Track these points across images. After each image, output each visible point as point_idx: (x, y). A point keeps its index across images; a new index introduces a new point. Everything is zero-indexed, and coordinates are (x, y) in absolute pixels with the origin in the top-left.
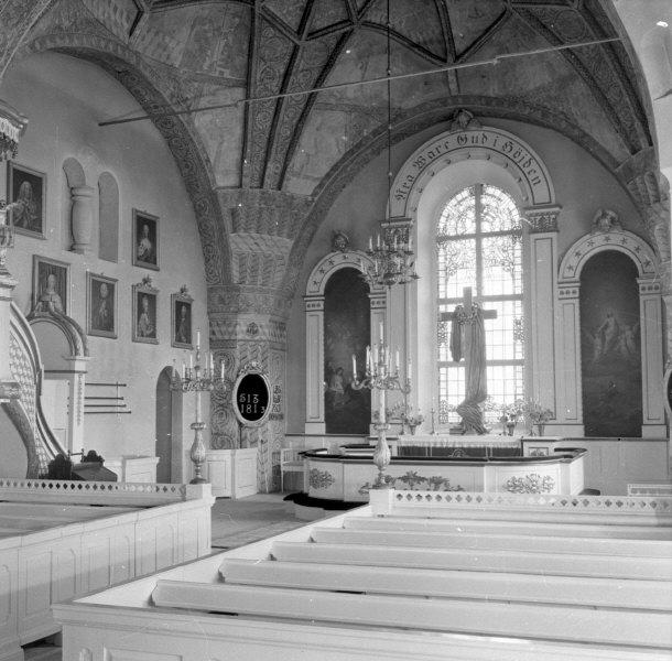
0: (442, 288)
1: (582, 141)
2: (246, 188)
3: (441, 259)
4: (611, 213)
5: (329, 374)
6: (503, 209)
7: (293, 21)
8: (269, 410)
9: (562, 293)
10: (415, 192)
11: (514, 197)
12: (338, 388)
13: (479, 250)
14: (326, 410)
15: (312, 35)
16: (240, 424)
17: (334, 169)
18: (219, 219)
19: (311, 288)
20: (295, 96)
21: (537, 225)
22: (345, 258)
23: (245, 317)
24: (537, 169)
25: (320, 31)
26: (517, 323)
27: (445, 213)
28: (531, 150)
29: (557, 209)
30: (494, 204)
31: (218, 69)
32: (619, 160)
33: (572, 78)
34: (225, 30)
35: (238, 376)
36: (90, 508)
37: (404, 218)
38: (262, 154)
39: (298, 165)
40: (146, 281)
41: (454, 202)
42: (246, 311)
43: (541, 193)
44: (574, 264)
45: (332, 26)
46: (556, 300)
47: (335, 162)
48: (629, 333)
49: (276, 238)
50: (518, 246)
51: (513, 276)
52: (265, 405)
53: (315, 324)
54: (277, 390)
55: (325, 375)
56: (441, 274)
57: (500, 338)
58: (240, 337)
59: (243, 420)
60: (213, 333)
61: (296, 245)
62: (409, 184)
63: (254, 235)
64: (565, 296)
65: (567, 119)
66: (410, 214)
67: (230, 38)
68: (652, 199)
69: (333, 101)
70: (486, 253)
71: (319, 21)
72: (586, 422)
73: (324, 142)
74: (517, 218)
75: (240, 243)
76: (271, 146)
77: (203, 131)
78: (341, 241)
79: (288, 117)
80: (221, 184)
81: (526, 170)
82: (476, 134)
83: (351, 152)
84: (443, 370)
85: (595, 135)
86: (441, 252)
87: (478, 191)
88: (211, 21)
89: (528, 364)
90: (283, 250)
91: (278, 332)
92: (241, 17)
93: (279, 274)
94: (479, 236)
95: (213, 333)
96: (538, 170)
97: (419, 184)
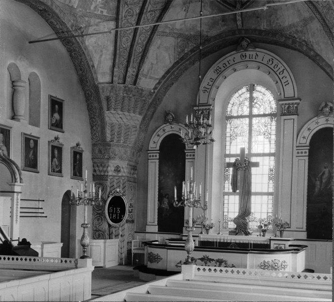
0: (228, 148)
2: (115, 84)
3: (228, 130)
6: (266, 100)
8: (126, 216)
9: (298, 153)
10: (214, 88)
11: (273, 92)
12: (166, 205)
13: (250, 125)
16: (110, 226)
18: (100, 102)
19: (152, 145)
21: (286, 110)
23: (113, 161)
24: (288, 76)
26: (271, 170)
27: (231, 102)
28: (285, 65)
30: (261, 97)
31: (100, 9)
33: (311, 19)
35: (108, 197)
38: (125, 63)
41: (237, 95)
42: (114, 158)
43: (289, 91)
44: (307, 136)
46: (294, 157)
49: (132, 114)
50: (274, 123)
51: (270, 141)
54: (131, 206)
56: (228, 139)
57: (261, 179)
58: (110, 173)
59: (111, 223)
61: (144, 119)
62: (211, 83)
63: (120, 112)
64: (300, 155)
65: (307, 45)
66: (211, 102)
69: (168, 31)
70: (255, 127)
72: (159, 224)
74: (274, 106)
75: (112, 117)
81: (281, 76)
82: (251, 53)
83: (176, 63)
84: (226, 197)
86: (228, 126)
87: (252, 89)
89: (276, 196)
91: (132, 171)
94: (251, 116)
95: (95, 171)
96: (288, 77)
97: (217, 84)
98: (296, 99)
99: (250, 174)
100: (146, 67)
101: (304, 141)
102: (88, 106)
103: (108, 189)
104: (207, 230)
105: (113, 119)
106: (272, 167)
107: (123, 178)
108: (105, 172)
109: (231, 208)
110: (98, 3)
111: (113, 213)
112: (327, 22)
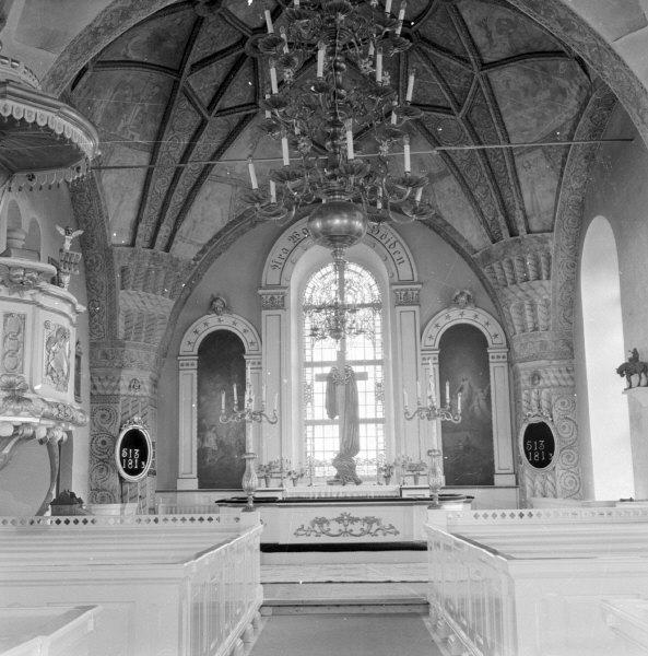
0: (308, 352)
1: (440, 228)
4: (468, 292)
5: (202, 430)
6: (363, 285)
7: (206, 98)
8: (147, 467)
10: (288, 263)
12: (211, 443)
14: (198, 466)
15: (221, 112)
17: (217, 236)
18: (110, 274)
19: (184, 347)
20: (192, 169)
21: (401, 297)
22: (220, 320)
24: (401, 250)
25: (228, 109)
27: (311, 285)
28: (397, 235)
29: (420, 286)
30: (356, 279)
31: (130, 132)
32: (477, 248)
33: (442, 175)
34: (142, 97)
35: (120, 430)
36: (392, 579)
37: (279, 286)
39: (185, 231)
40: (462, 314)
41: (319, 275)
42: (129, 367)
43: (405, 272)
44: (435, 334)
45: (239, 106)
47: (218, 230)
48: (480, 394)
50: (378, 317)
51: (374, 344)
52: (145, 460)
53: (188, 379)
55: (198, 431)
58: (123, 392)
59: (125, 475)
60: (95, 387)
62: (284, 256)
66: (284, 283)
67: (146, 105)
68: (509, 281)
71: (227, 101)
72: (200, 476)
73: (211, 211)
74: (377, 293)
75: (129, 301)
76: (165, 209)
77: (107, 189)
78: (217, 304)
79: (184, 184)
80: (115, 242)
81: (392, 251)
83: (232, 223)
85: (456, 225)
86: (307, 320)
88: (132, 87)
90: (166, 310)
92: (161, 87)
93: (159, 332)
95: (95, 387)
97: (292, 257)
98: (415, 284)
99: (354, 390)
100: (185, 226)
101: (189, 348)
102: (88, 280)
103: (120, 417)
104: (294, 480)
105: (131, 303)
106: (379, 381)
107: (143, 400)
108: (114, 389)
109: (318, 445)
110: (128, 123)
111: (533, 451)
112: (467, 182)
